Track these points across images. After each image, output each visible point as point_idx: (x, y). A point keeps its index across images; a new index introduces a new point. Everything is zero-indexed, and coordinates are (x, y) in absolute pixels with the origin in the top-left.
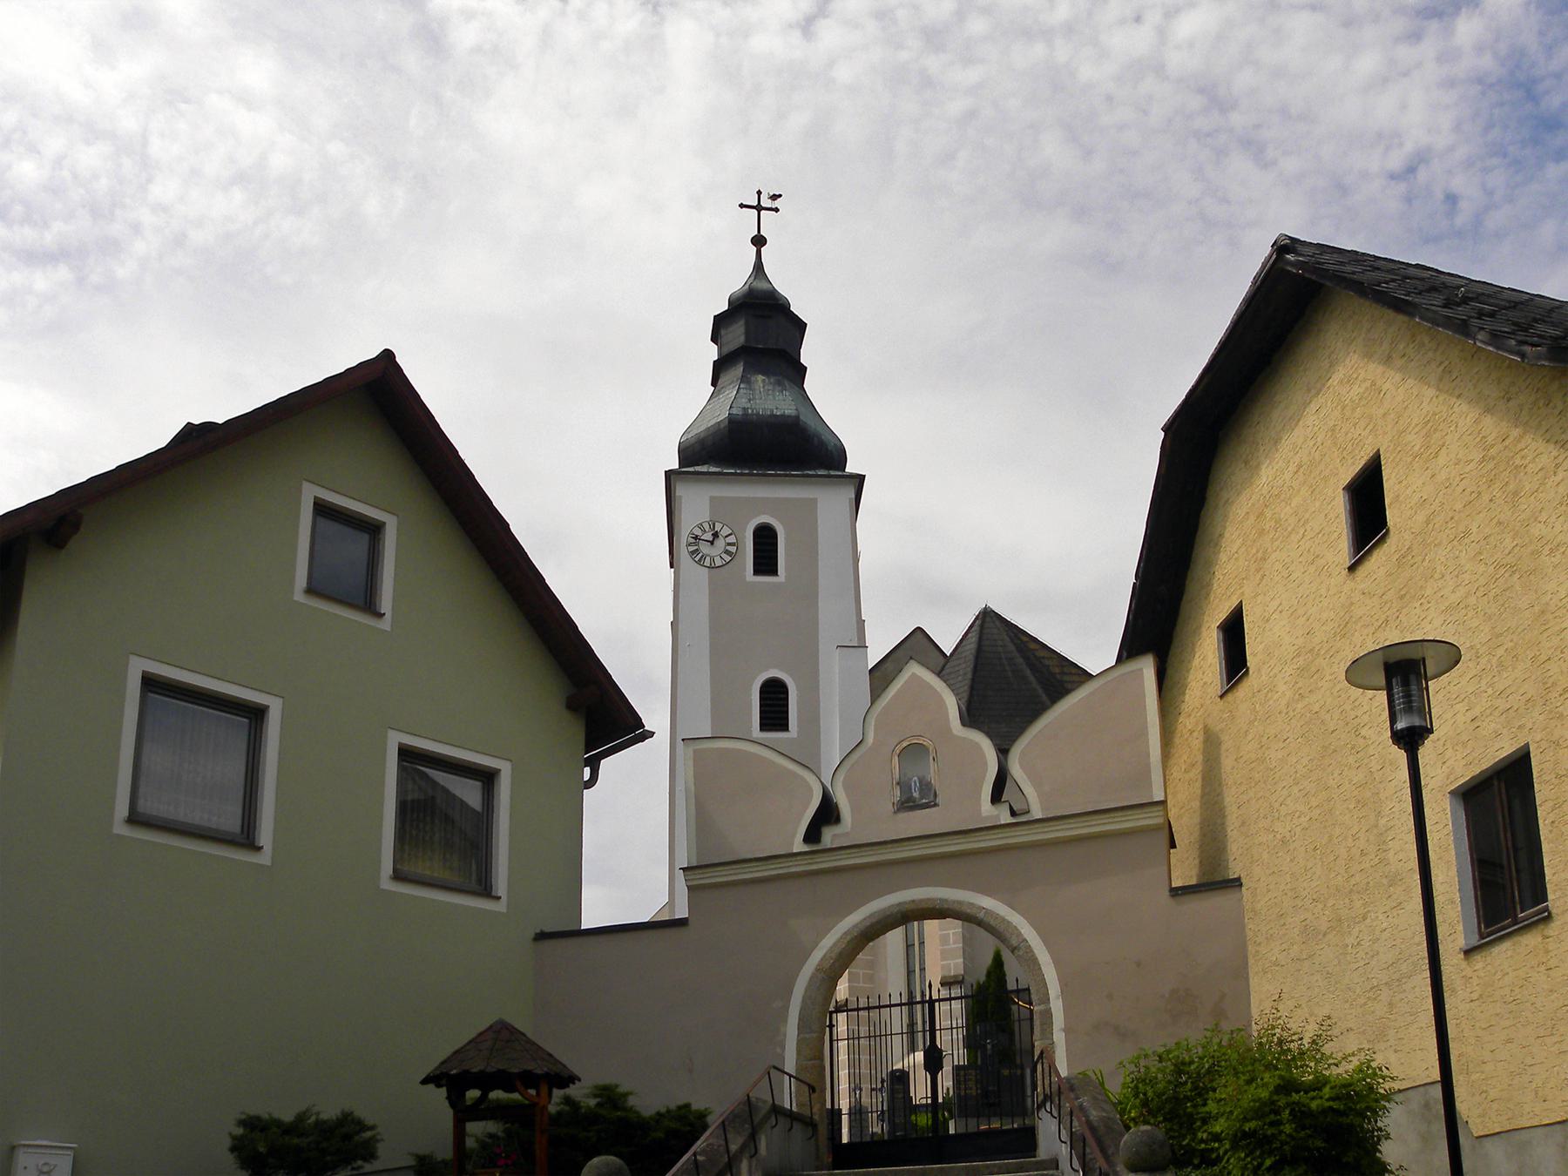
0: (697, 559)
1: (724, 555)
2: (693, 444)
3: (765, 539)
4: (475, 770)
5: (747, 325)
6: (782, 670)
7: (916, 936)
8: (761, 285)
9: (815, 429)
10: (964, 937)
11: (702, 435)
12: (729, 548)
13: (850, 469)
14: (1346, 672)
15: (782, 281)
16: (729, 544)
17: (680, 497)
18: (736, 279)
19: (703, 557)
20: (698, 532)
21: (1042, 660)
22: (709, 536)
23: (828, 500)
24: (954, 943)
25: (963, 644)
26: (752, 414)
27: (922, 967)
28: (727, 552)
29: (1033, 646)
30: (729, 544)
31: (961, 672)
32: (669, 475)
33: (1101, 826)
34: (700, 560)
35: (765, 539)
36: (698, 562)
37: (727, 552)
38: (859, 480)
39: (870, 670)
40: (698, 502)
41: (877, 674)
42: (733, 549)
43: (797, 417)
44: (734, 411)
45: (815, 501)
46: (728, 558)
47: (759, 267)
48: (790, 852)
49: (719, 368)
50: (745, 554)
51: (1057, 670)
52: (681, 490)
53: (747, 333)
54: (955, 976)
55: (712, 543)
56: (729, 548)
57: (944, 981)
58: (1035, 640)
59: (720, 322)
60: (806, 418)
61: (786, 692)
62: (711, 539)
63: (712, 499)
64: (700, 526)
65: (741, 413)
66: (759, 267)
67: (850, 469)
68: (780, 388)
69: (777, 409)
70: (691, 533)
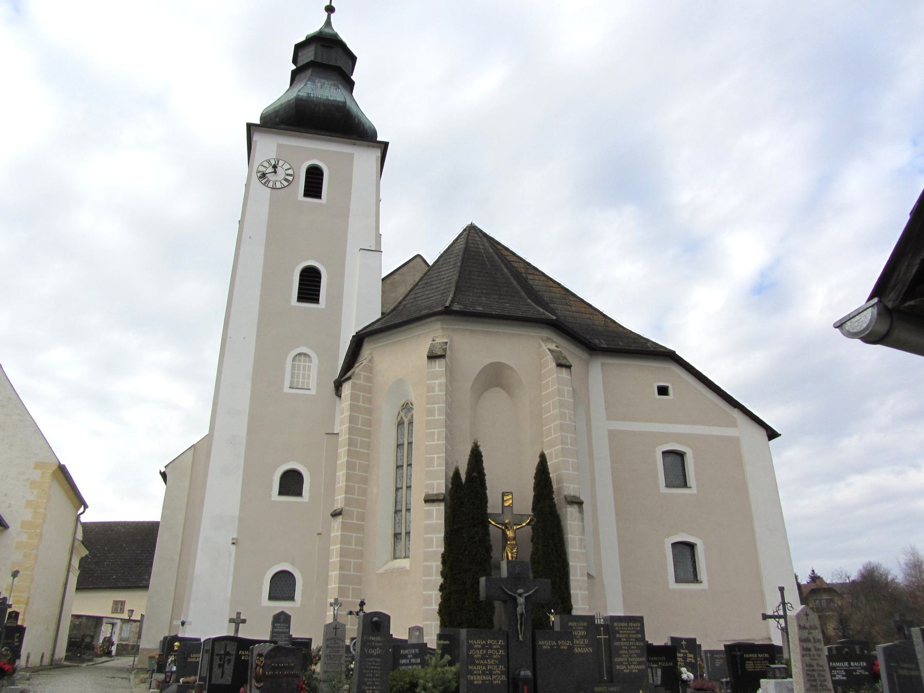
0: (263, 182)
2: (270, 114)
5: (316, 50)
6: (320, 160)
7: (404, 503)
8: (327, 30)
9: (357, 113)
10: (446, 460)
11: (277, 109)
12: (287, 177)
15: (343, 30)
16: (288, 175)
17: (256, 142)
18: (315, 26)
19: (268, 181)
21: (512, 263)
22: (271, 170)
23: (365, 157)
24: (438, 466)
25: (454, 246)
26: (314, 97)
27: (407, 531)
28: (286, 180)
29: (505, 253)
30: (288, 175)
31: (452, 263)
34: (265, 183)
36: (264, 184)
37: (286, 180)
38: (385, 146)
39: (383, 280)
41: (388, 281)
42: (290, 178)
43: (345, 103)
44: (301, 94)
46: (286, 184)
47: (328, 23)
49: (294, 74)
50: (299, 182)
51: (523, 271)
53: (316, 55)
54: (437, 495)
55: (275, 172)
56: (287, 177)
57: (428, 499)
58: (507, 249)
59: (299, 48)
60: (349, 103)
61: (322, 174)
62: (273, 171)
63: (279, 145)
65: (305, 95)
66: (328, 23)
68: (335, 87)
69: (331, 96)
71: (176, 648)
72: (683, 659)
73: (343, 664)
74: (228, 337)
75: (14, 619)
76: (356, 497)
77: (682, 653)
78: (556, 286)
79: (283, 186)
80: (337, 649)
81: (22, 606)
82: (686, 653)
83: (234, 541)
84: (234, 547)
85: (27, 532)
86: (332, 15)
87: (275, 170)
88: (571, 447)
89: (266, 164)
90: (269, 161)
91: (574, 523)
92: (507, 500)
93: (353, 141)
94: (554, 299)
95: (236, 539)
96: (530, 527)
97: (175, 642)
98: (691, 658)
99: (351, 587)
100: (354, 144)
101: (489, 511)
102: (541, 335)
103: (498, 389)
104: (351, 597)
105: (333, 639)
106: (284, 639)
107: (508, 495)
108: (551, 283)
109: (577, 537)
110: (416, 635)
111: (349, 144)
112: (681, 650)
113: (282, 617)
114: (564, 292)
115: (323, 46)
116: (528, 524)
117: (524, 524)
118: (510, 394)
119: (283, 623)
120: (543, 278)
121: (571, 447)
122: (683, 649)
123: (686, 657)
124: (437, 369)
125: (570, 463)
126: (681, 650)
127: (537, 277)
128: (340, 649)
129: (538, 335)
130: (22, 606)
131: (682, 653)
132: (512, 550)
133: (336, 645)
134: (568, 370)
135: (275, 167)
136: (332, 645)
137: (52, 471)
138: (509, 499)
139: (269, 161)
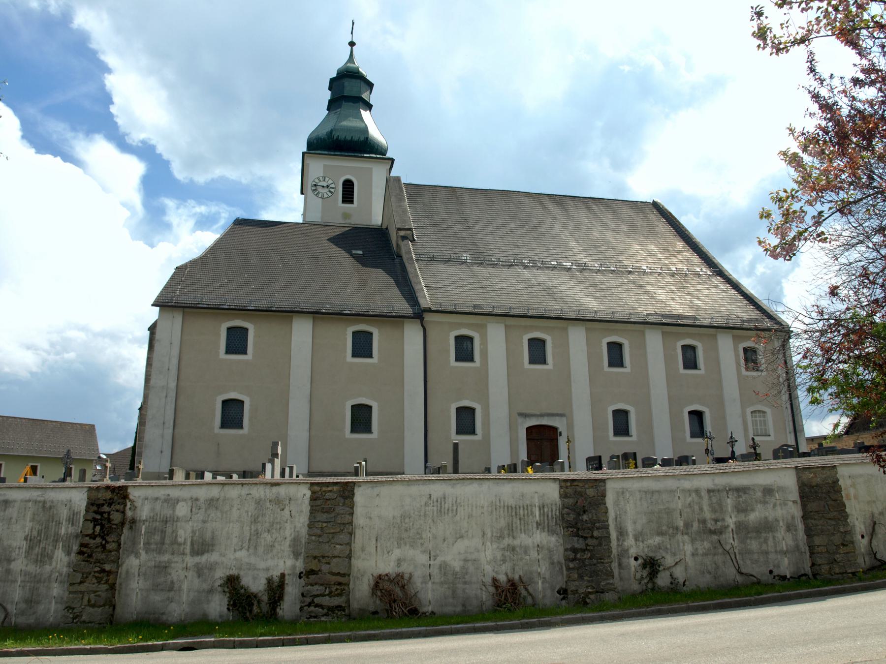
1: (328, 193)
3: (348, 186)
4: (632, 617)
13: (388, 155)
14: (655, 205)
15: (354, 40)
17: (308, 164)
20: (317, 181)
32: (304, 154)
33: (275, 473)
35: (348, 186)
37: (330, 191)
40: (319, 166)
45: (372, 168)
46: (330, 194)
48: (358, 95)
52: (307, 161)
63: (325, 166)
64: (318, 178)
67: (388, 155)
70: (314, 181)
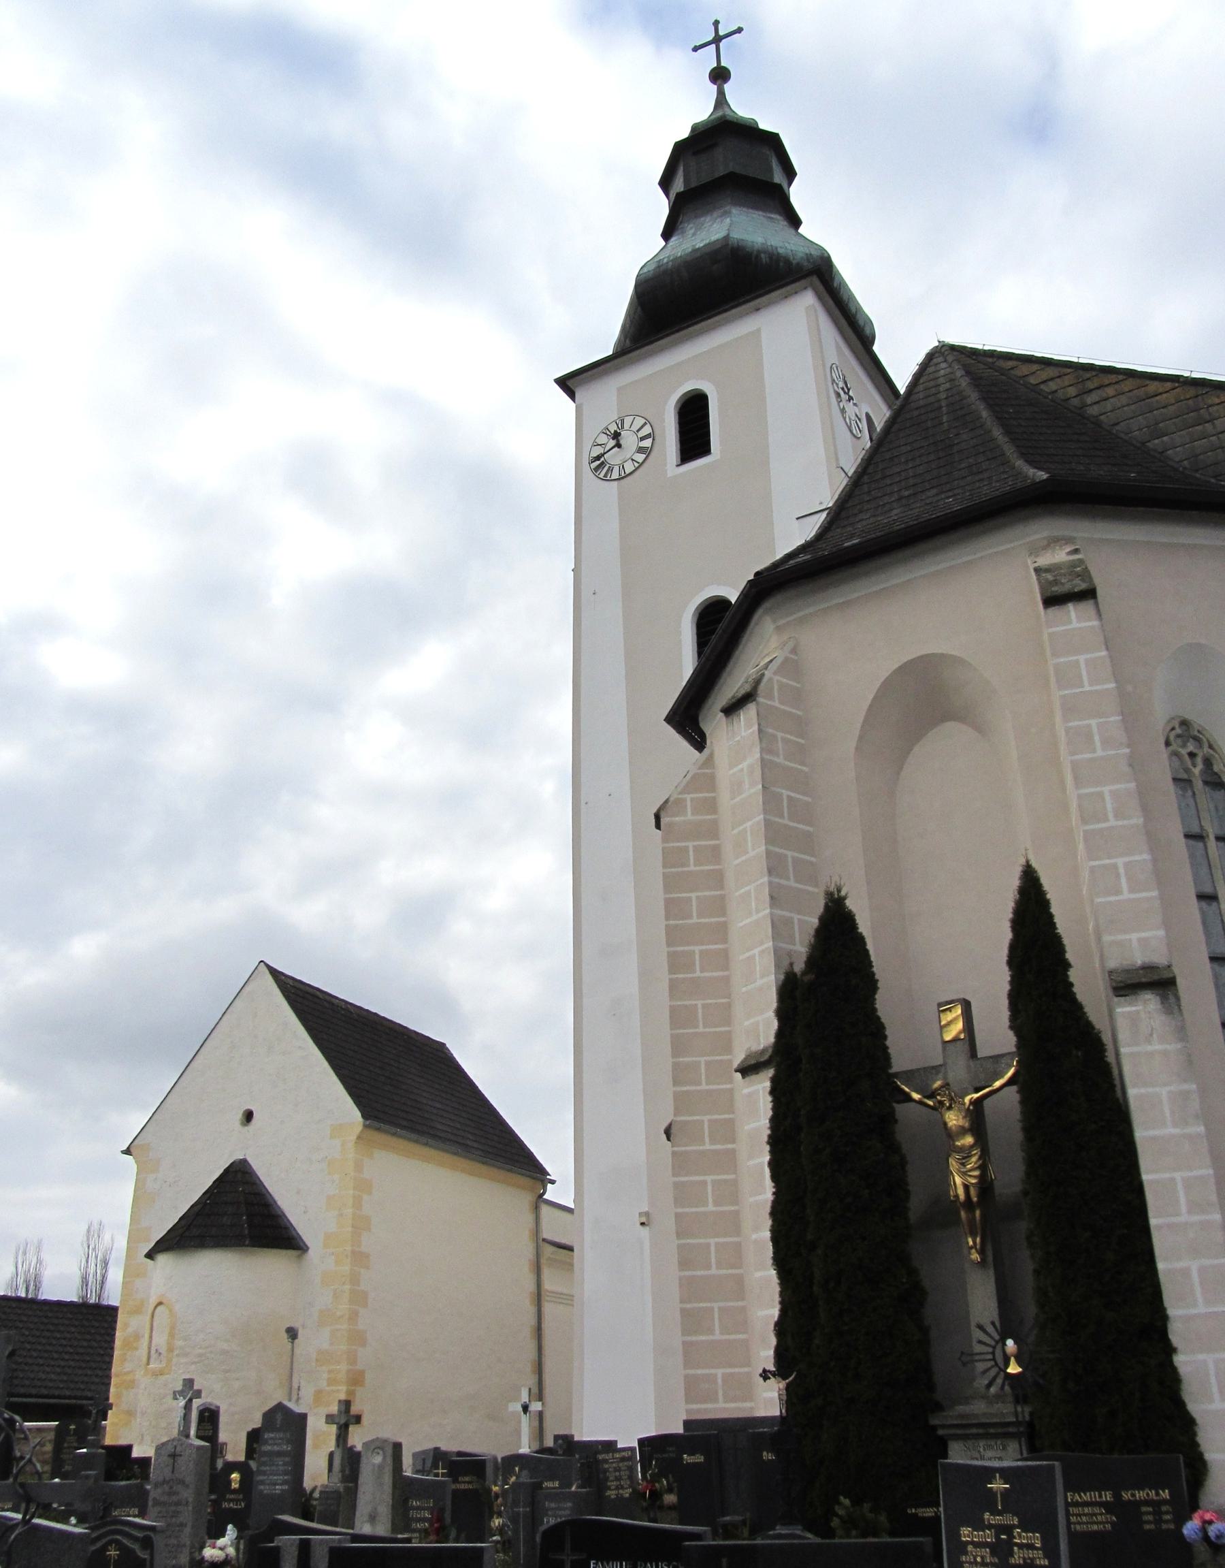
16: (642, 439)
21: (1125, 377)
28: (641, 450)
30: (642, 439)
34: (605, 476)
37: (641, 450)
46: (640, 457)
47: (721, 101)
55: (619, 445)
66: (721, 101)
71: (235, 1485)
72: (993, 1553)
73: (184, 1545)
74: (583, 802)
75: (208, 1422)
76: (704, 1087)
77: (990, 1527)
78: (1169, 385)
79: (637, 465)
80: (173, 1508)
81: (340, 1388)
82: (1008, 1530)
83: (644, 1220)
84: (645, 1232)
85: (333, 1254)
86: (727, 87)
87: (618, 441)
88: (1120, 823)
89: (603, 439)
90: (605, 432)
91: (1149, 1048)
92: (949, 1024)
93: (752, 304)
94: (1160, 425)
95: (647, 1214)
96: (1014, 1088)
97: (233, 1473)
98: (1031, 1547)
99: (716, 1305)
100: (758, 310)
101: (899, 1064)
102: (1028, 540)
103: (950, 725)
104: (717, 1332)
105: (168, 1482)
106: (281, 1468)
107: (949, 1010)
108: (1153, 387)
109: (1164, 1092)
110: (374, 1465)
111: (747, 314)
112: (987, 1516)
113: (279, 1417)
114: (1192, 392)
115: (695, 153)
116: (1010, 1082)
117: (997, 1084)
118: (981, 729)
119: (278, 1430)
120: (1129, 384)
121: (1120, 823)
122: (995, 1512)
123: (1010, 1543)
124: (743, 734)
125: (1122, 871)
126: (987, 1516)
127: (1110, 391)
128: (180, 1508)
129: (1021, 542)
130: (340, 1388)
131: (990, 1527)
132: (964, 1165)
133: (175, 1498)
134: (1087, 607)
135: (616, 436)
136: (165, 1498)
137: (355, 1137)
138: (955, 1019)
139: (605, 432)
